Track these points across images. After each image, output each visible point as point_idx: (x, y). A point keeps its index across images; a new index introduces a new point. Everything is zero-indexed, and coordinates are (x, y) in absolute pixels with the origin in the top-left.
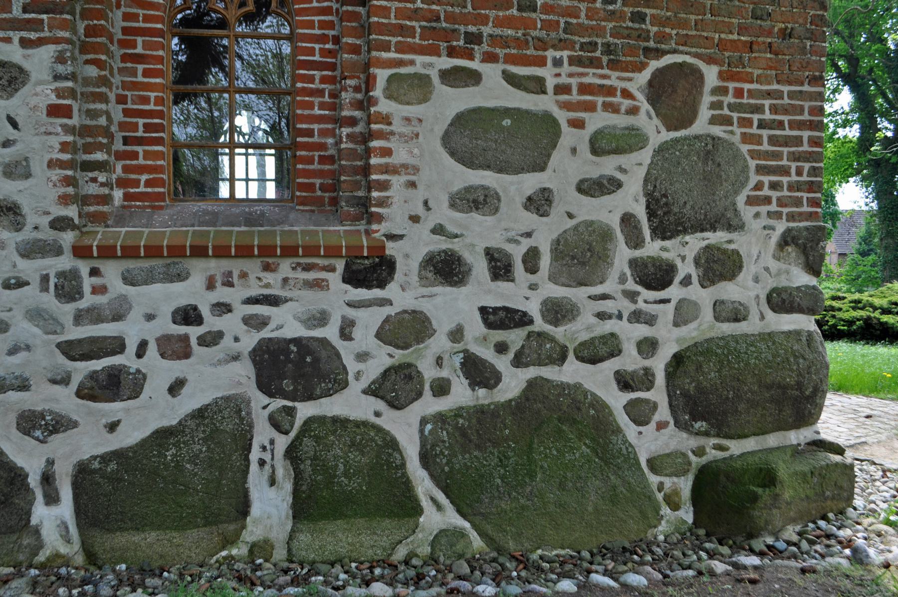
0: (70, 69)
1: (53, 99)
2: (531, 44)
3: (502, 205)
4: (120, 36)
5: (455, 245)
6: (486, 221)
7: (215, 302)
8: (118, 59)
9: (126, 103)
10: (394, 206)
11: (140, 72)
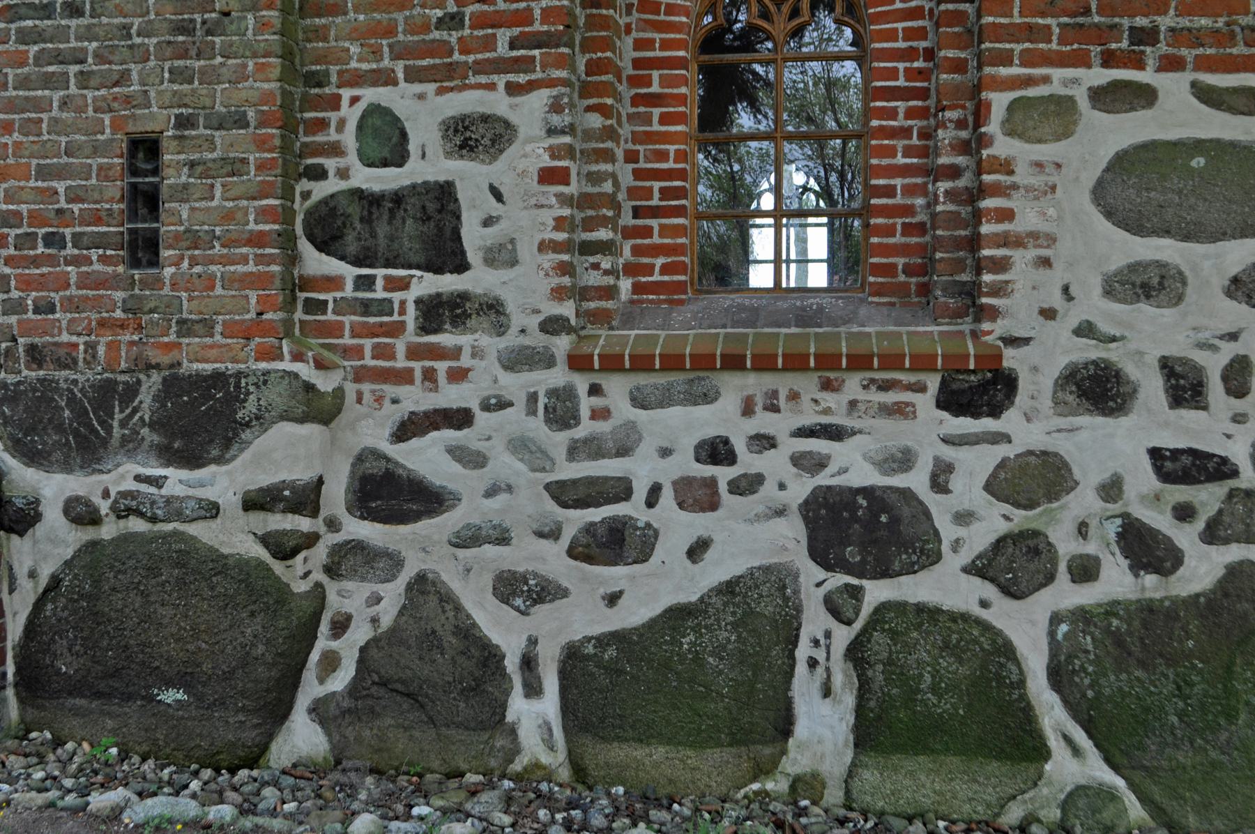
1: (547, 161)
2: (1239, 37)
3: (1189, 290)
5: (1112, 353)
6: (1163, 316)
7: (753, 433)
8: (627, 101)
9: (637, 161)
10: (1017, 295)
11: (656, 119)
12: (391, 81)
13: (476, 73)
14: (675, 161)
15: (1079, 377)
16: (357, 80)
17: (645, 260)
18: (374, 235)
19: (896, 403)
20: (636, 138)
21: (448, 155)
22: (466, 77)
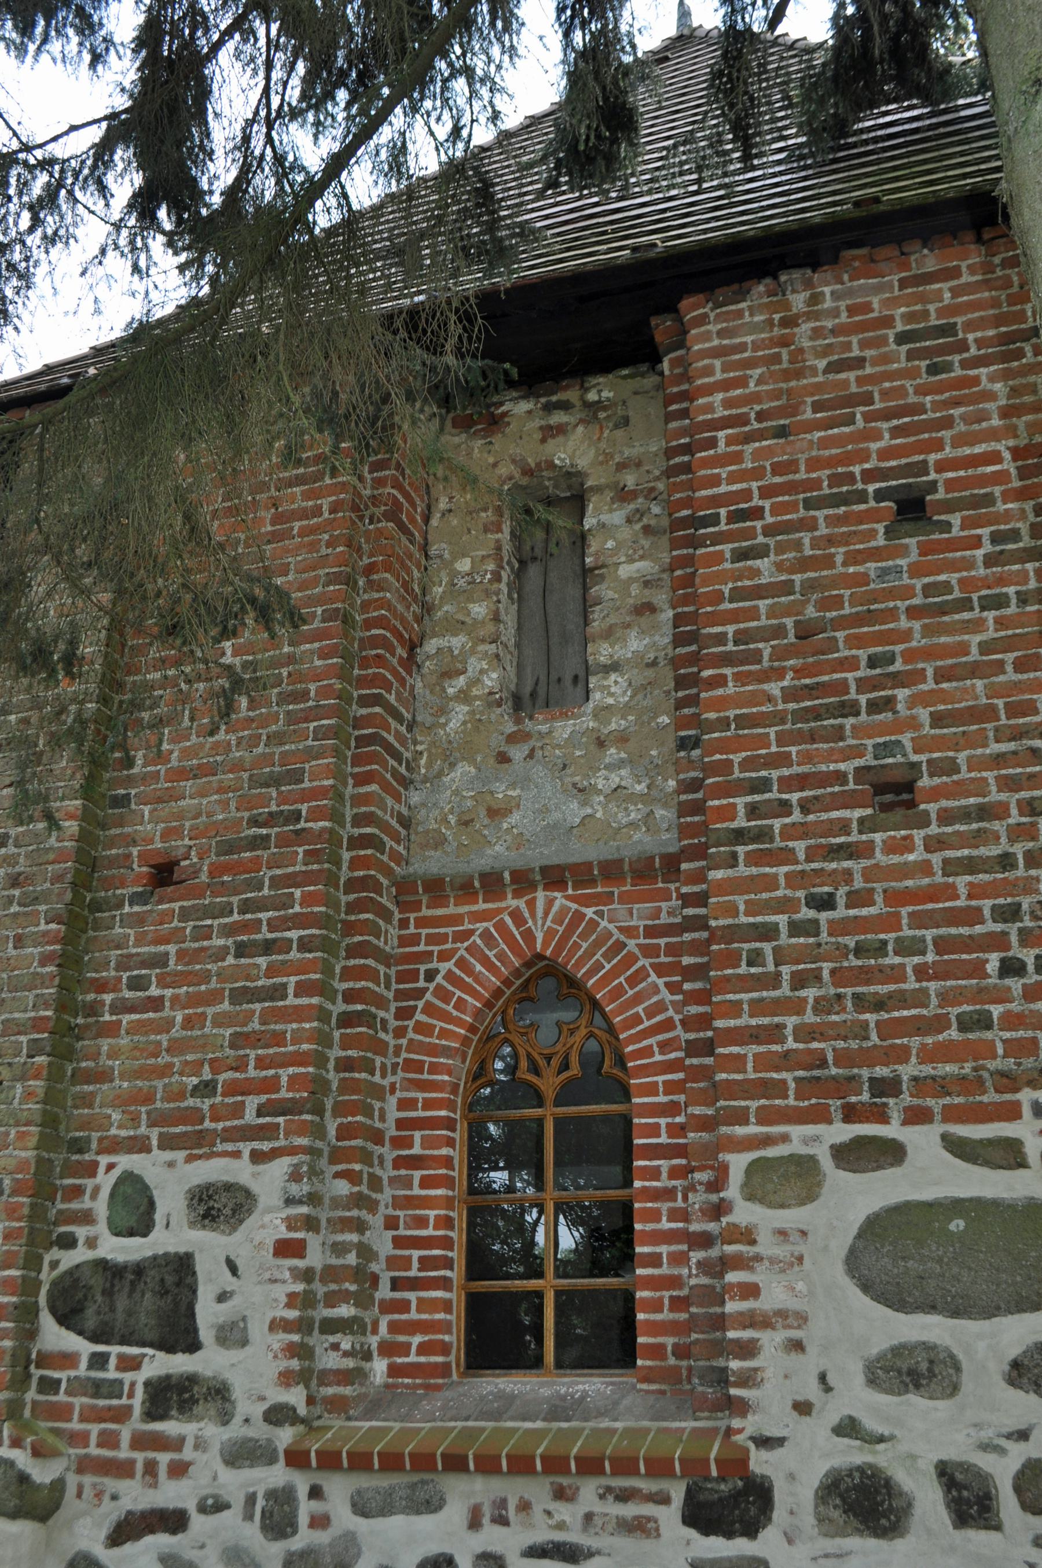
0: (306, 1189)
1: (284, 1233)
2: (989, 1084)
3: (965, 1377)
4: (393, 1132)
5: (880, 1457)
6: (936, 1409)
7: (479, 1550)
8: (389, 1164)
9: (397, 1228)
10: (767, 1385)
11: (416, 1182)
12: (146, 1149)
13: (224, 1140)
14: (435, 1228)
15: (843, 1487)
16: (113, 1146)
17: (402, 1338)
18: (112, 1309)
19: (636, 1518)
20: (399, 1203)
21: (192, 1225)
22: (214, 1145)
